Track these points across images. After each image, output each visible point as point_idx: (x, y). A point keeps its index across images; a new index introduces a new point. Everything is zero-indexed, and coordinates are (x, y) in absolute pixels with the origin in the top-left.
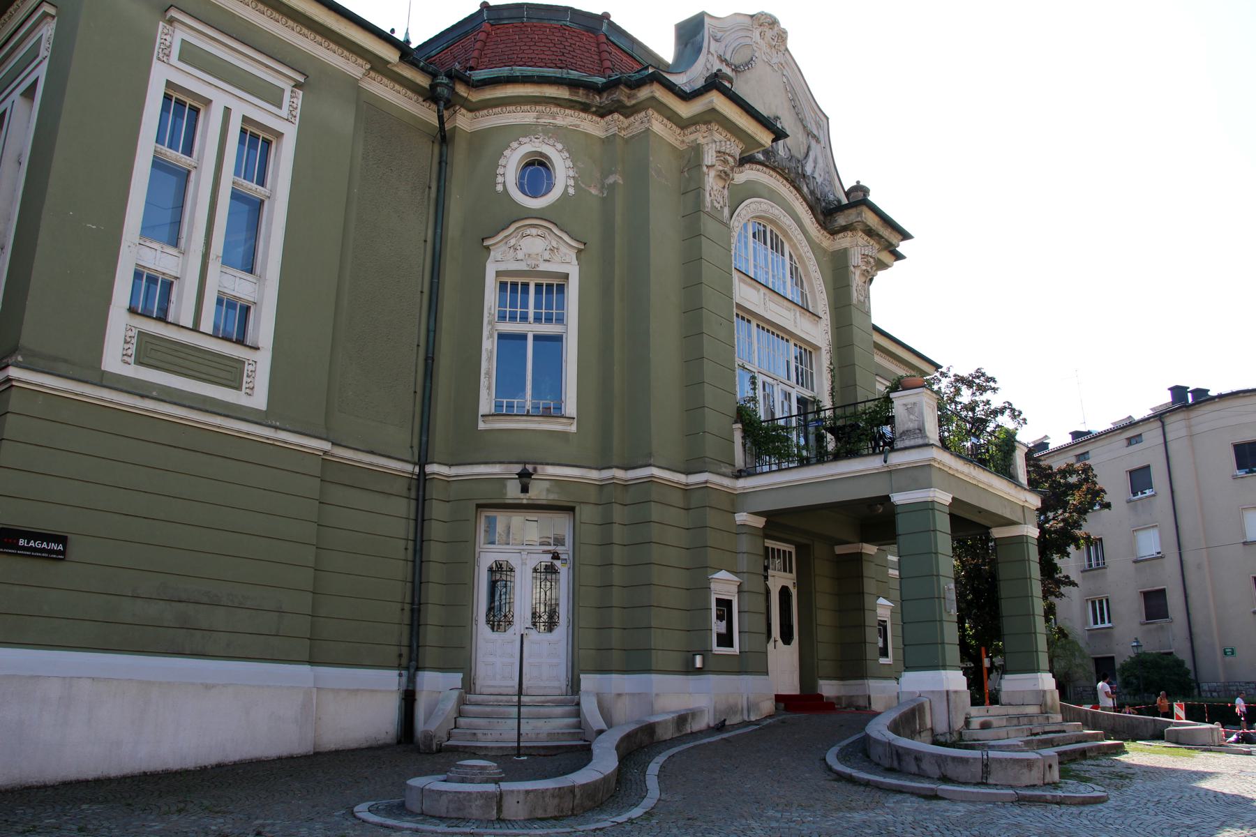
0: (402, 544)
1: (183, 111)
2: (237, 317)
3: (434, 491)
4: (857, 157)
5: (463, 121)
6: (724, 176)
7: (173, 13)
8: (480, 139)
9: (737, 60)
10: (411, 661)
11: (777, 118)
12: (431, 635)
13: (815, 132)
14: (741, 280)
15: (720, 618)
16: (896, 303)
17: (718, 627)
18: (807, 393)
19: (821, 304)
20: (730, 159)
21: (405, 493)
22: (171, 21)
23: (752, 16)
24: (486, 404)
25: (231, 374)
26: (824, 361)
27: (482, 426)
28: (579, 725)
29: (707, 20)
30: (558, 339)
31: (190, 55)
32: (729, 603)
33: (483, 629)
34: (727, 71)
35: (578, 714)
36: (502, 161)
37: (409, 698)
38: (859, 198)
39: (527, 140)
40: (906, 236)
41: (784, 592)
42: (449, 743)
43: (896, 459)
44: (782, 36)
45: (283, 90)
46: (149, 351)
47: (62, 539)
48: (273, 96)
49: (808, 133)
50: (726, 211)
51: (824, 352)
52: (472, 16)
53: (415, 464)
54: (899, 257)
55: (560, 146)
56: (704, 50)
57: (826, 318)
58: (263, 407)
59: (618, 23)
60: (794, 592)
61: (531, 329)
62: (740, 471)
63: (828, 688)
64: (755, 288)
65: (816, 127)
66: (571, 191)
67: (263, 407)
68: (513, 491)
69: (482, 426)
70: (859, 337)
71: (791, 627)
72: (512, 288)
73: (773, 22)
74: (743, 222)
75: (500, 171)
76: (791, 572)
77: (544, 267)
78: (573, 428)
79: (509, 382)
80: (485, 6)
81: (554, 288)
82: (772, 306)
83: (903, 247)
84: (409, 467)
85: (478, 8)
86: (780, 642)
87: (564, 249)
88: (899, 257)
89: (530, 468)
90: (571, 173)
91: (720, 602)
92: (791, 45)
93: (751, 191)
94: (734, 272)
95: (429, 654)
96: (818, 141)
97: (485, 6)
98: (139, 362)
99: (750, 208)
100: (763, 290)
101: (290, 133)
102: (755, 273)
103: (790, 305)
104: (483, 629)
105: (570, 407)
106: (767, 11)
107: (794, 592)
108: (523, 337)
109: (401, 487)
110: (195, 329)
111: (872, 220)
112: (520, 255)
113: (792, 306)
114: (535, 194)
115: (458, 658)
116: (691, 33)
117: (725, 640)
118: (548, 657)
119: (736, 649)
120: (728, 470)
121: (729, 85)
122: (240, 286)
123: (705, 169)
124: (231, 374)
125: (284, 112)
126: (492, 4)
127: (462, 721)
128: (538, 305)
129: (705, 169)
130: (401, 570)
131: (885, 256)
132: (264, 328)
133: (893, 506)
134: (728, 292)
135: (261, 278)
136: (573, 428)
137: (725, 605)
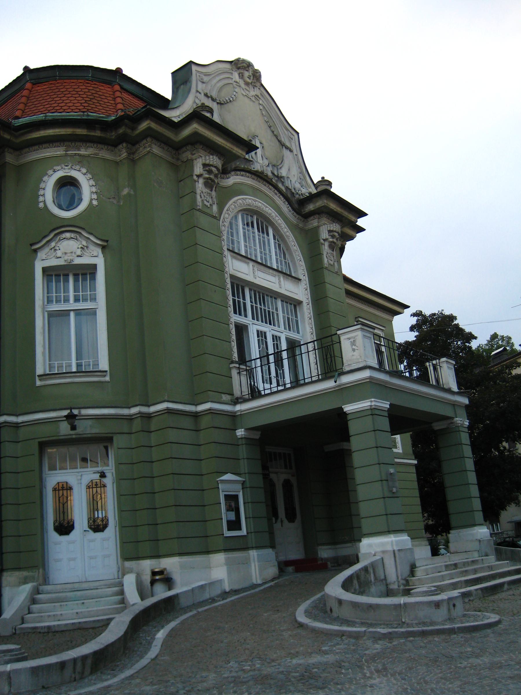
4: (327, 158)
6: (209, 184)
9: (224, 96)
11: (255, 136)
13: (288, 144)
14: (233, 257)
15: (229, 509)
16: (360, 261)
17: (226, 516)
18: (294, 336)
19: (301, 270)
20: (214, 169)
23: (231, 62)
26: (307, 311)
27: (38, 383)
29: (194, 68)
32: (236, 497)
33: (53, 536)
34: (208, 103)
35: (122, 593)
36: (42, 185)
38: (324, 189)
39: (59, 168)
40: (362, 214)
41: (287, 484)
42: (24, 626)
43: (345, 379)
44: (257, 75)
49: (282, 145)
50: (215, 208)
51: (305, 304)
52: (18, 78)
54: (361, 230)
55: (84, 170)
56: (193, 90)
59: (129, 75)
60: (294, 481)
62: (237, 399)
63: (325, 553)
64: (245, 262)
65: (286, 138)
66: (95, 203)
68: (64, 428)
69: (38, 383)
70: (335, 292)
74: (232, 215)
75: (41, 192)
76: (291, 468)
77: (78, 261)
78: (107, 378)
80: (26, 69)
83: (361, 222)
85: (22, 72)
86: (285, 521)
88: (361, 230)
89: (75, 412)
91: (227, 497)
92: (264, 81)
93: (236, 191)
94: (226, 253)
96: (291, 151)
97: (26, 69)
99: (236, 203)
100: (251, 264)
102: (246, 252)
103: (274, 272)
104: (53, 536)
105: (104, 364)
106: (242, 57)
107: (294, 481)
111: (333, 206)
113: (277, 273)
114: (68, 209)
116: (182, 76)
119: (244, 532)
121: (208, 115)
123: (195, 178)
126: (32, 67)
127: (35, 607)
128: (76, 290)
131: (350, 232)
133: (345, 414)
134: (221, 269)
136: (107, 378)
137: (232, 499)
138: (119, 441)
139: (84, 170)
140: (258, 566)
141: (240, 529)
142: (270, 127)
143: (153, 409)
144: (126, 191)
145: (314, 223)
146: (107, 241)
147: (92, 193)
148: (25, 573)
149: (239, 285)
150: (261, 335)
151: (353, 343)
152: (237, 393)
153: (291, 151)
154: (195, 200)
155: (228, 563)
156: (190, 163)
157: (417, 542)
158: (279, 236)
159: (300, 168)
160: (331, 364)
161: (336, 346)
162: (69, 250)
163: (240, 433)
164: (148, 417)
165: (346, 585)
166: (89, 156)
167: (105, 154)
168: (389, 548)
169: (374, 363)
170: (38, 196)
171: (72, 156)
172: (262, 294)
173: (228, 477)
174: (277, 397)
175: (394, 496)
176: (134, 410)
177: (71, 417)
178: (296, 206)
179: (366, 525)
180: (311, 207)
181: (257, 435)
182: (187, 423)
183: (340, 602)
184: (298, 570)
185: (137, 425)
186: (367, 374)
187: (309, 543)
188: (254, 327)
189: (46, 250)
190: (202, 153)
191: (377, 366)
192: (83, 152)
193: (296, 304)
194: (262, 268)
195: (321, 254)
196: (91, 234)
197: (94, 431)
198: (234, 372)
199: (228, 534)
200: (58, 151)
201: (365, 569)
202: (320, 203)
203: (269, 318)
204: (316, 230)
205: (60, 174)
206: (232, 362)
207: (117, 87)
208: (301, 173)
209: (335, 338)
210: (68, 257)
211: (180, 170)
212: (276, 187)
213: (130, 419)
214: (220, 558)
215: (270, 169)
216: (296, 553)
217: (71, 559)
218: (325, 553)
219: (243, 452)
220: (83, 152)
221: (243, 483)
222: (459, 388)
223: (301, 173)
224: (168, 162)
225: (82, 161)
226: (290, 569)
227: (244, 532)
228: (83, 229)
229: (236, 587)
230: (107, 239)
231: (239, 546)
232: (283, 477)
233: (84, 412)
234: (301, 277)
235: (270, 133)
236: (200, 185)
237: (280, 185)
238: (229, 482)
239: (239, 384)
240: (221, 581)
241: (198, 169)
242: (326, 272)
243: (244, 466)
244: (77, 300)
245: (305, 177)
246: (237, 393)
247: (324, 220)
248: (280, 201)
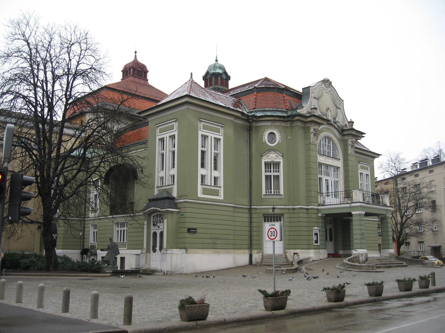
3: (253, 211)
5: (254, 124)
10: (250, 248)
12: (254, 242)
17: (315, 238)
24: (264, 192)
25: (216, 193)
26: (341, 170)
27: (263, 197)
28: (287, 260)
37: (251, 256)
41: (330, 229)
44: (330, 83)
46: (205, 192)
47: (196, 229)
49: (337, 108)
51: (341, 168)
61: (272, 174)
63: (341, 252)
66: (280, 141)
67: (222, 198)
69: (263, 197)
71: (332, 237)
72: (268, 165)
73: (328, 81)
77: (275, 160)
79: (268, 187)
81: (278, 164)
82: (327, 160)
84: (248, 207)
87: (279, 156)
90: (280, 137)
95: (254, 246)
98: (203, 194)
100: (325, 157)
105: (282, 192)
108: (271, 176)
110: (211, 186)
111: (354, 133)
112: (270, 158)
115: (260, 248)
117: (316, 242)
118: (279, 248)
119: (319, 244)
120: (316, 204)
124: (216, 193)
128: (274, 168)
132: (221, 182)
133: (352, 214)
135: (220, 172)
137: (316, 234)
138: (286, 215)
140: (323, 254)
144: (289, 137)
145: (346, 138)
149: (321, 164)
150: (327, 180)
151: (356, 194)
152: (319, 203)
154: (310, 141)
155: (315, 253)
156: (309, 128)
158: (334, 143)
159: (343, 115)
161: (351, 194)
162: (272, 157)
163: (320, 215)
165: (349, 260)
167: (283, 124)
168: (361, 253)
169: (362, 201)
173: (316, 228)
175: (364, 239)
177: (274, 209)
179: (355, 246)
180: (346, 133)
181: (324, 216)
186: (359, 204)
187: (336, 248)
188: (324, 178)
189: (266, 156)
191: (362, 201)
192: (277, 124)
194: (328, 157)
198: (319, 196)
199: (315, 244)
200: (269, 124)
201: (354, 258)
202: (349, 132)
204: (347, 140)
208: (343, 117)
212: (334, 127)
213: (289, 209)
214: (312, 251)
215: (333, 120)
216: (332, 252)
218: (341, 252)
219: (320, 220)
220: (277, 124)
222: (390, 204)
223: (343, 117)
225: (276, 127)
226: (331, 256)
227: (319, 244)
229: (316, 259)
231: (318, 248)
232: (330, 227)
233: (277, 207)
234: (340, 158)
236: (312, 135)
238: (316, 229)
241: (312, 130)
242: (349, 156)
243: (320, 225)
244: (274, 172)
246: (319, 203)
247: (350, 137)
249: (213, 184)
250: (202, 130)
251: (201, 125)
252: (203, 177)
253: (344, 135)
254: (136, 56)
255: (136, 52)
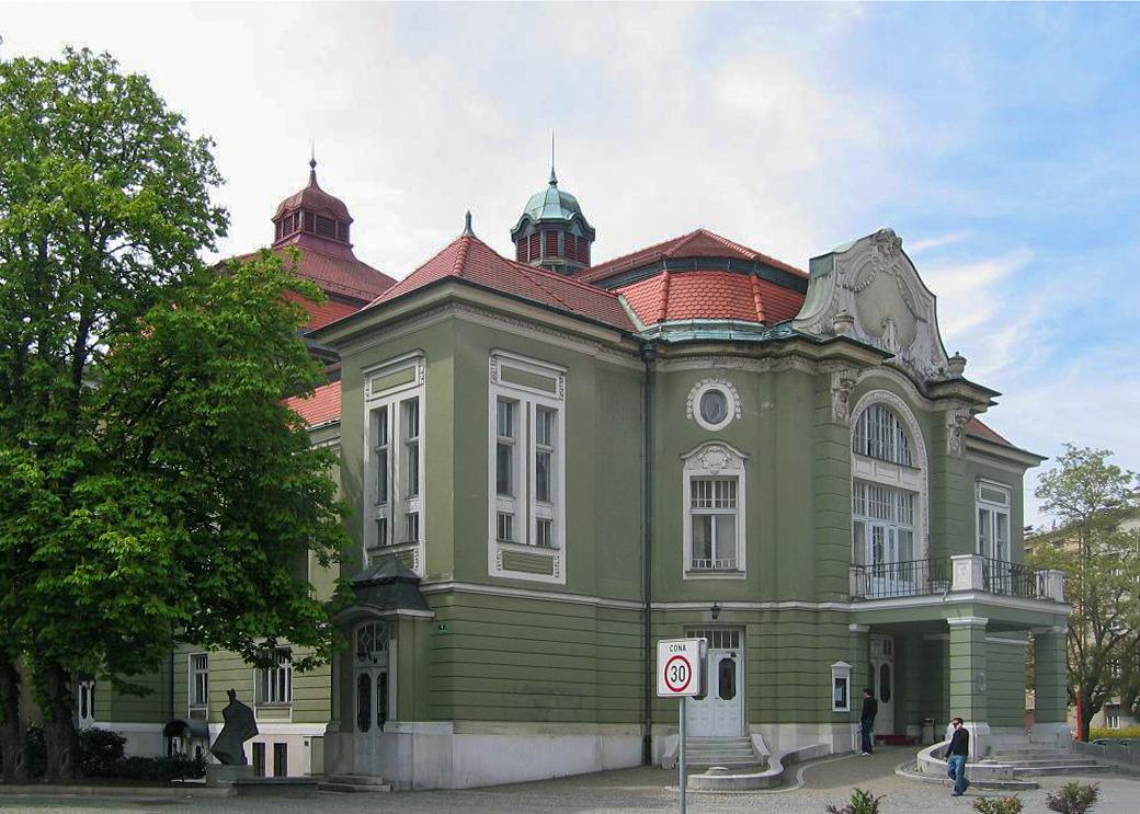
0: (638, 651)
1: (508, 406)
2: (544, 526)
3: (655, 618)
5: (660, 367)
7: (683, 457)
8: (668, 376)
13: (923, 316)
17: (835, 693)
19: (921, 458)
21: (638, 620)
22: (495, 356)
24: (687, 565)
25: (546, 566)
26: (923, 502)
28: (752, 753)
30: (733, 517)
31: (508, 375)
37: (647, 741)
41: (885, 669)
45: (555, 380)
46: (509, 561)
48: (549, 386)
49: (916, 318)
51: (921, 494)
53: (643, 603)
57: (925, 468)
58: (564, 582)
60: (891, 666)
62: (853, 598)
66: (738, 416)
69: (685, 577)
72: (699, 485)
75: (689, 404)
78: (745, 577)
89: (718, 605)
96: (925, 321)
101: (561, 406)
105: (742, 565)
107: (891, 666)
109: (636, 617)
110: (528, 544)
117: (841, 704)
122: (546, 512)
123: (832, 392)
124: (546, 566)
125: (557, 395)
129: (832, 392)
130: (639, 666)
132: (559, 536)
137: (841, 682)
139: (729, 385)
141: (845, 706)
142: (905, 301)
143: (781, 605)
144: (767, 405)
145: (941, 406)
146: (748, 454)
147: (736, 406)
148: (669, 727)
149: (860, 483)
153: (925, 321)
157: (997, 730)
160: (939, 573)
162: (715, 462)
163: (853, 627)
164: (777, 611)
166: (734, 369)
170: (686, 407)
171: (718, 369)
172: (880, 489)
173: (840, 664)
174: (890, 597)
176: (764, 605)
177: (716, 610)
178: (924, 390)
180: (940, 392)
182: (810, 617)
183: (929, 763)
184: (888, 743)
185: (767, 617)
190: (841, 367)
193: (912, 495)
195: (945, 441)
196: (736, 448)
197: (733, 620)
199: (835, 710)
200: (706, 364)
203: (884, 513)
205: (707, 387)
206: (852, 565)
207: (754, 279)
208: (934, 345)
209: (949, 561)
210: (715, 469)
211: (819, 384)
213: (761, 611)
217: (722, 719)
219: (854, 643)
221: (851, 670)
224: (809, 375)
225: (728, 375)
228: (729, 443)
230: (749, 451)
232: (882, 662)
235: (905, 308)
236: (836, 399)
237: (910, 371)
238: (840, 668)
239: (855, 584)
240: (826, 746)
241: (836, 383)
245: (937, 348)
246: (853, 592)
247: (954, 404)
248: (908, 387)
249: (533, 541)
250: (499, 381)
251: (495, 368)
252: (505, 521)
253: (935, 399)
254: (313, 174)
255: (313, 164)
